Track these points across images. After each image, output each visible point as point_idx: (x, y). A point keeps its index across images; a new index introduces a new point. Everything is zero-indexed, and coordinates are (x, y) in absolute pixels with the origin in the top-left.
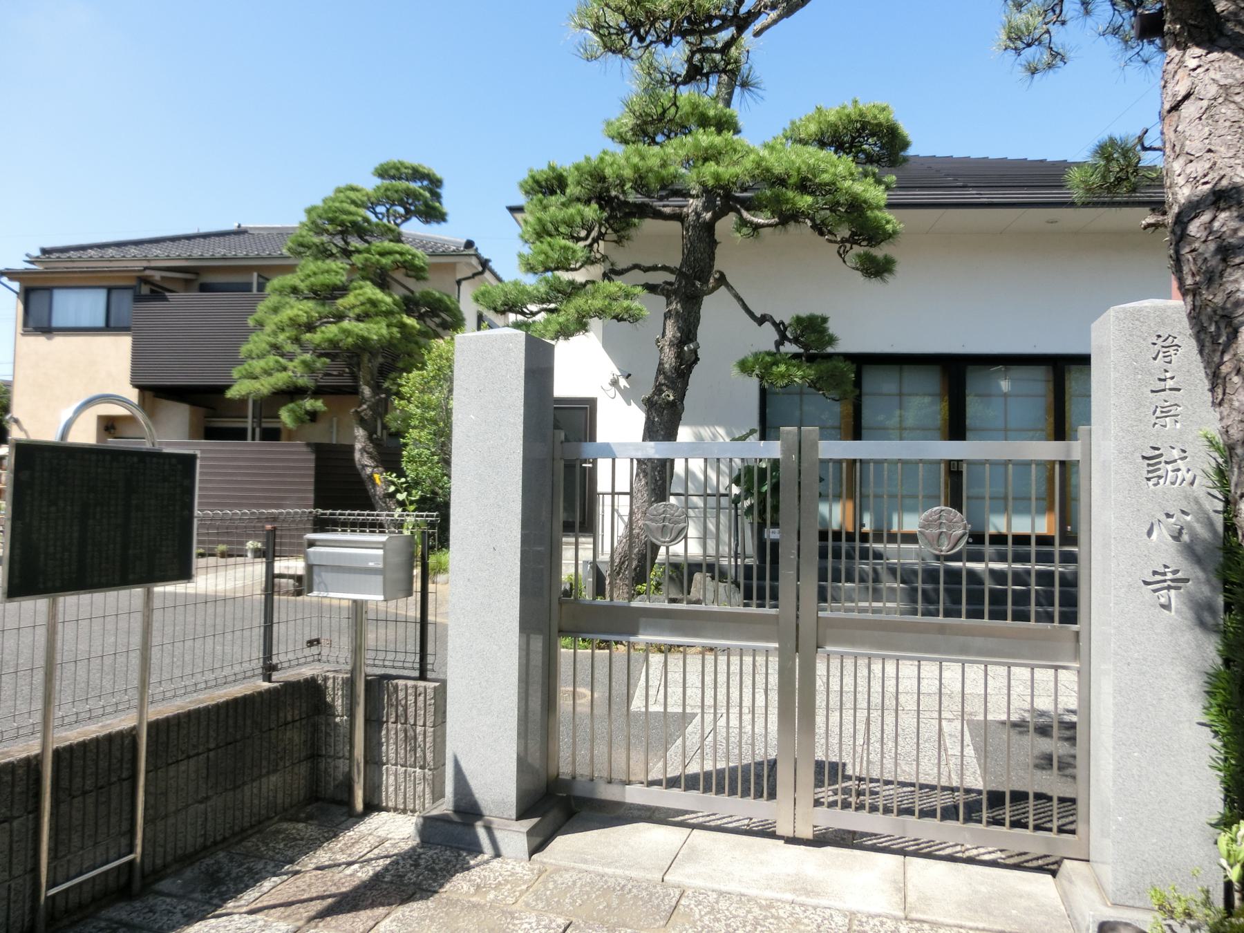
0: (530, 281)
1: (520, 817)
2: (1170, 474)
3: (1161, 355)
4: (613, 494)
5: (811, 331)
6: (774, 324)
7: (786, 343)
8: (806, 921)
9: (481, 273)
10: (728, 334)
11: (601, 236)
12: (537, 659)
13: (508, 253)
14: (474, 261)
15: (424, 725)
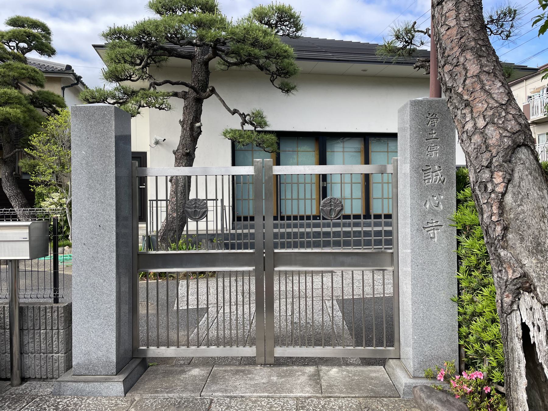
0: (111, 86)
1: (118, 372)
2: (434, 177)
3: (430, 122)
5: (258, 120)
6: (240, 115)
8: (275, 405)
9: (77, 84)
10: (217, 120)
11: (147, 65)
12: (125, 288)
13: (93, 72)
14: (71, 77)
15: (58, 329)
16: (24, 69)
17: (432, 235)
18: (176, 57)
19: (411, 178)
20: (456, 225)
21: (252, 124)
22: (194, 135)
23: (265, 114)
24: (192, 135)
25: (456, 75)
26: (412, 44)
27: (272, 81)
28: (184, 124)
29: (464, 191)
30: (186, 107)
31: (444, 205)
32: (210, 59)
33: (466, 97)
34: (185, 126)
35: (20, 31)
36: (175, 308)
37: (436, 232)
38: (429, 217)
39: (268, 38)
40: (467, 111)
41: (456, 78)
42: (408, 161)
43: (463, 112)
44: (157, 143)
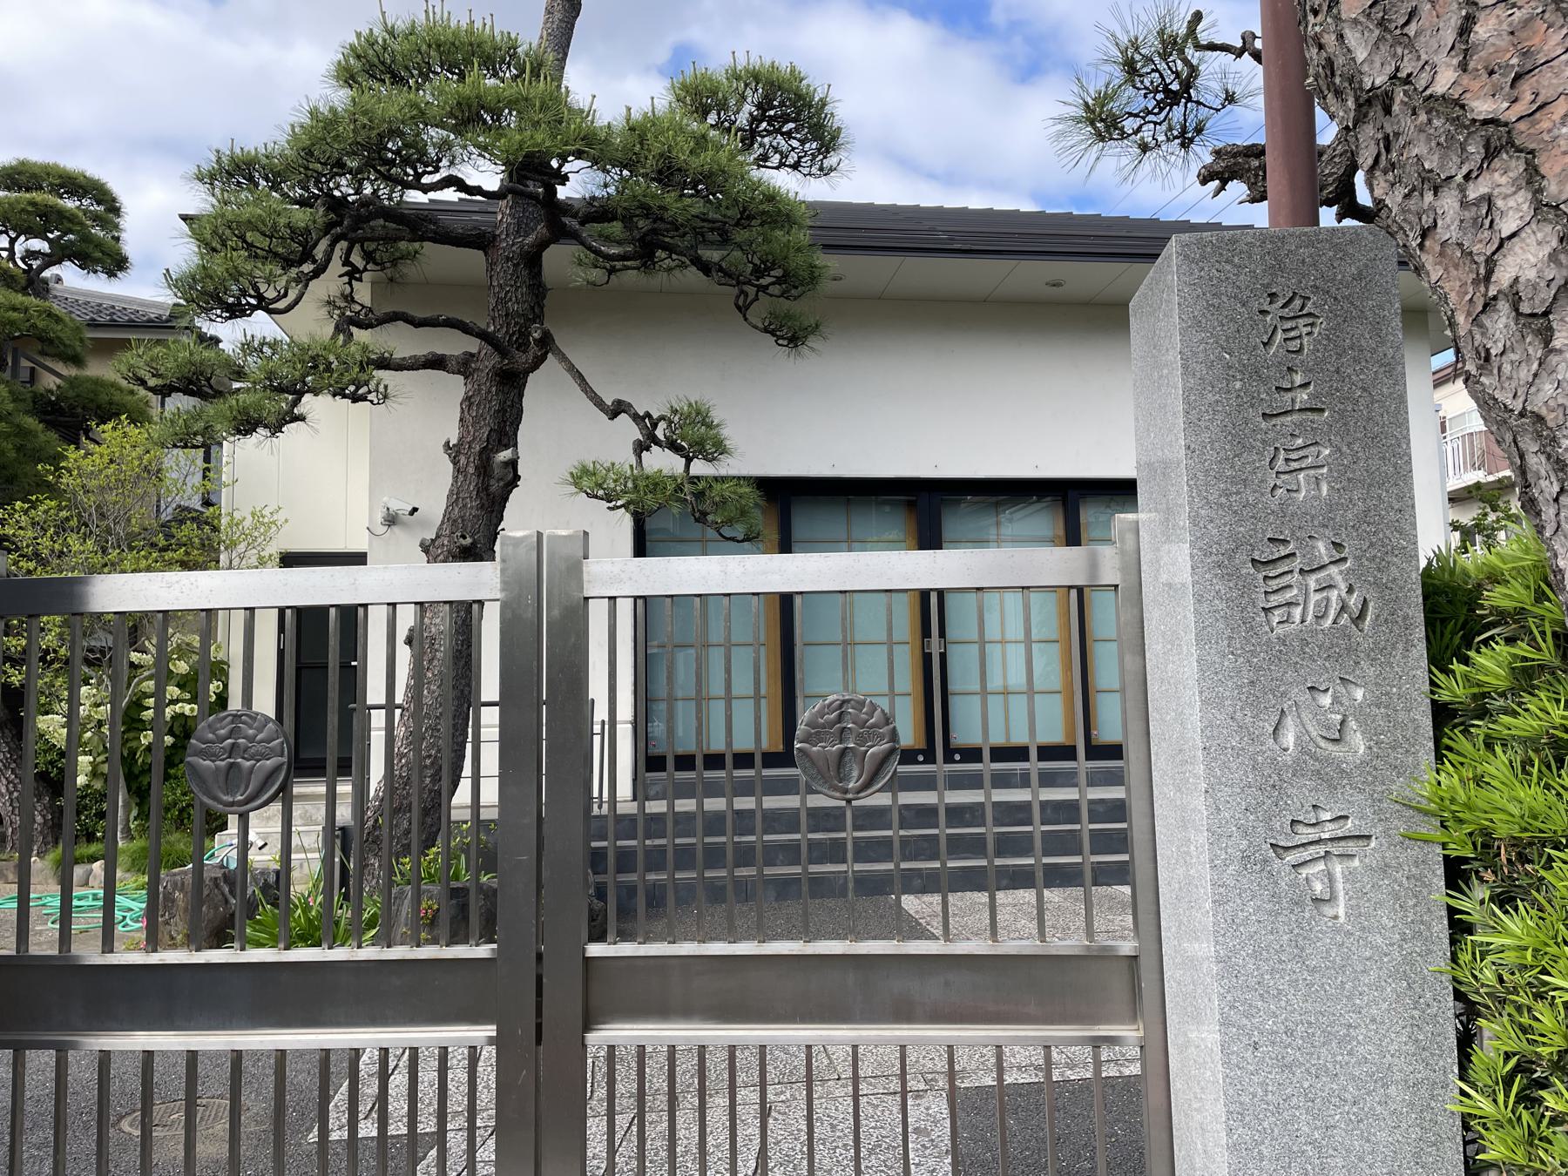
2: (1314, 598)
3: (1279, 336)
4: (1030, 692)
6: (637, 418)
7: (654, 448)
16: (15, 309)
17: (1318, 887)
18: (435, 241)
19: (1199, 599)
20: (1439, 835)
21: (673, 446)
22: (493, 489)
23: (716, 416)
24: (483, 489)
25: (1412, 14)
26: (1189, 99)
27: (742, 310)
28: (458, 453)
29: (1466, 661)
30: (468, 399)
31: (1371, 734)
32: (543, 245)
33: (1482, 107)
34: (463, 460)
35: (17, 201)
36: (313, 1137)
37: (1338, 869)
38: (1300, 796)
39: (706, 157)
40: (1501, 180)
41: (1412, 30)
42: (1184, 521)
43: (1475, 191)
44: (391, 520)
